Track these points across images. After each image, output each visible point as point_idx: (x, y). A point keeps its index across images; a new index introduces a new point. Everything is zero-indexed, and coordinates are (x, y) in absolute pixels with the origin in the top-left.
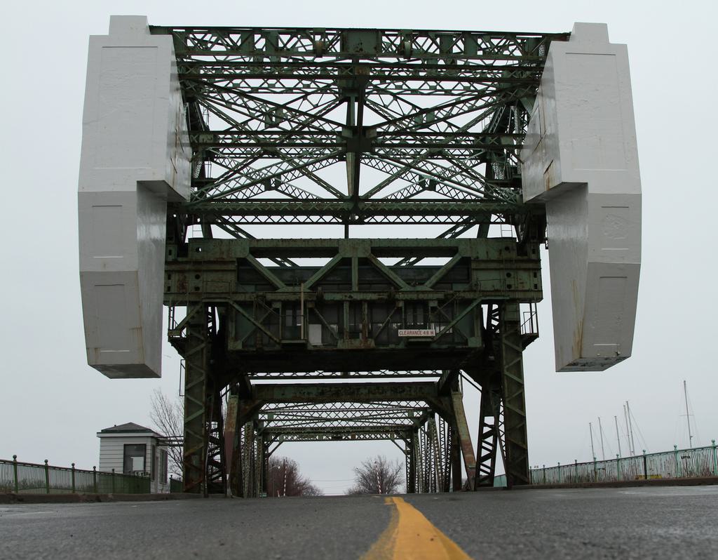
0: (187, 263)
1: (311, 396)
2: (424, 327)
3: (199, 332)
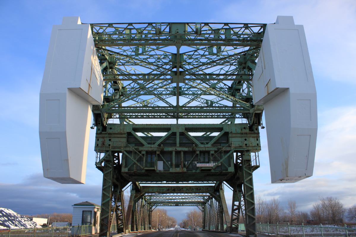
0: (105, 134)
1: (164, 191)
2: (209, 163)
3: (109, 164)
